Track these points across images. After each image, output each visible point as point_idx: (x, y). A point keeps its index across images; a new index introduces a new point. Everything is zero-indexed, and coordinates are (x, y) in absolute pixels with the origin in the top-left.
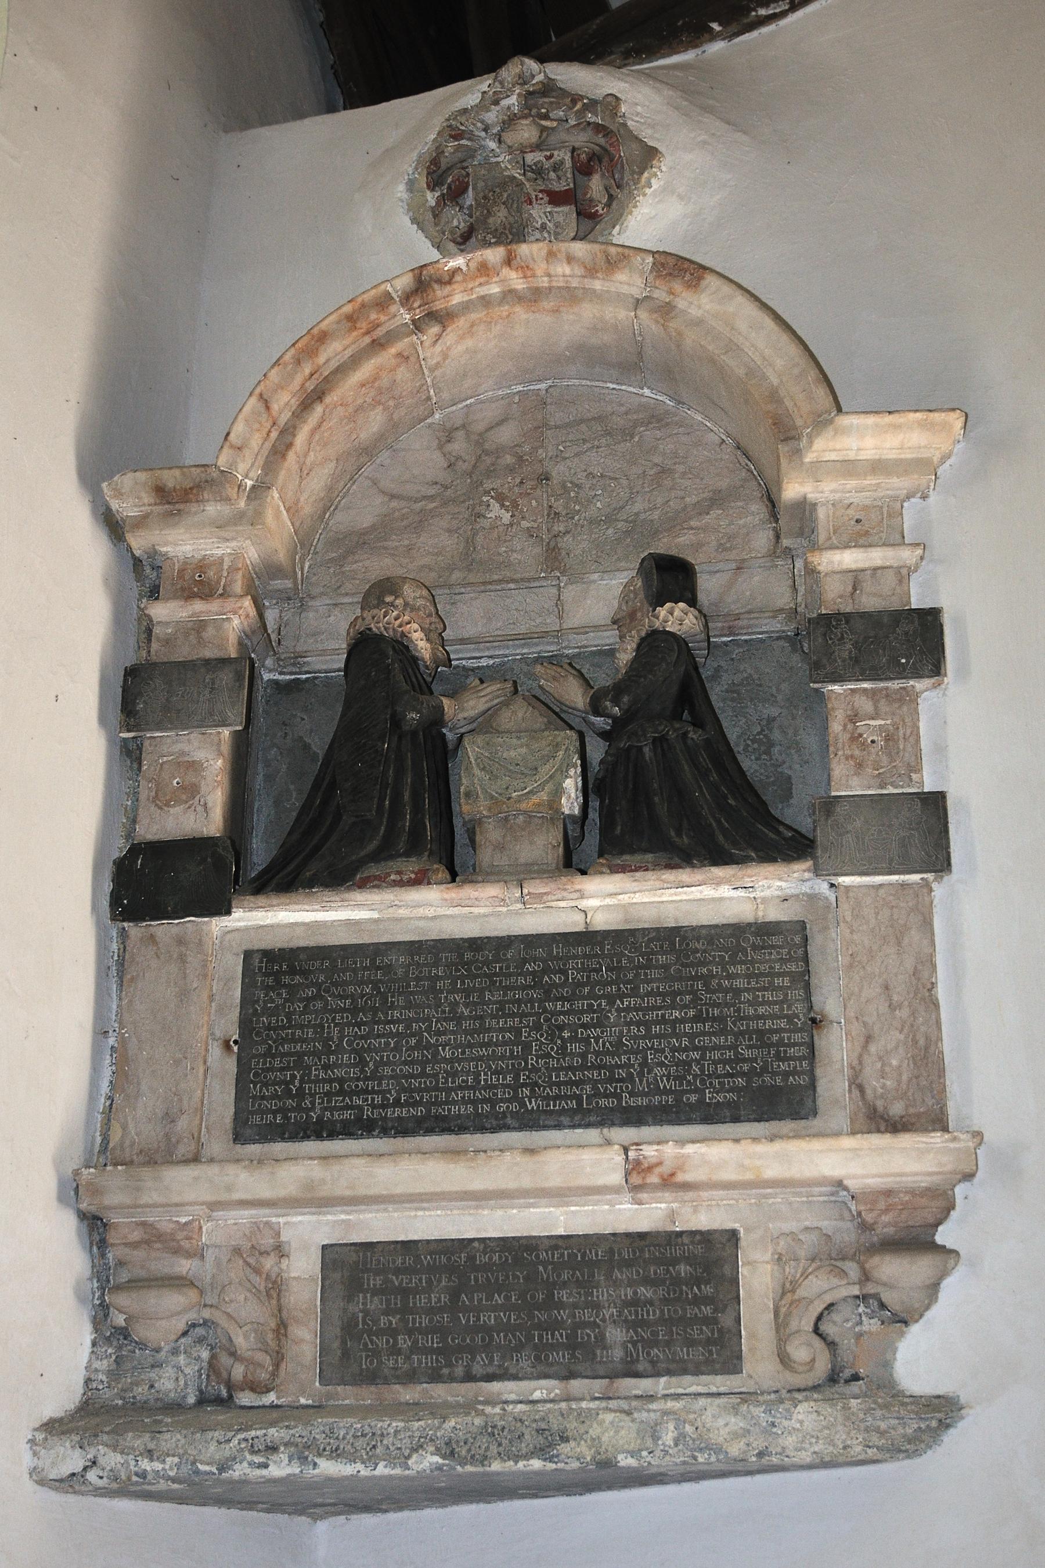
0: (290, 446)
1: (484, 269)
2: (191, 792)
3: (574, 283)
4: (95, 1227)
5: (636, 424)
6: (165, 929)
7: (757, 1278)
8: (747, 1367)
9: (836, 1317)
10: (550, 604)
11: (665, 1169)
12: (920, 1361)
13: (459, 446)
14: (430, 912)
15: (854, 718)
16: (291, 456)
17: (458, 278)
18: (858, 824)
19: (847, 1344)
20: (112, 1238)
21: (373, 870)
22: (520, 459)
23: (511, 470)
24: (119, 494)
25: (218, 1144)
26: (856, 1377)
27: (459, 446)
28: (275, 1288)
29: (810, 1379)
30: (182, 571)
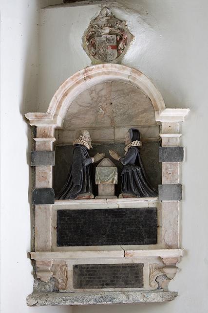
0: (61, 106)
1: (98, 68)
2: (45, 179)
3: (116, 71)
4: (33, 262)
5: (130, 92)
6: (42, 206)
7: (146, 272)
8: (144, 286)
9: (159, 278)
10: (112, 133)
11: (131, 255)
12: (172, 286)
13: (93, 95)
14: (90, 204)
15: (167, 169)
16: (61, 108)
17: (93, 70)
18: (166, 190)
19: (160, 283)
20: (37, 263)
21: (80, 195)
22: (106, 99)
23: (104, 101)
24: (28, 116)
25: (55, 247)
26: (162, 288)
27: (93, 95)
28: (66, 272)
29: (154, 289)
30: (41, 130)
